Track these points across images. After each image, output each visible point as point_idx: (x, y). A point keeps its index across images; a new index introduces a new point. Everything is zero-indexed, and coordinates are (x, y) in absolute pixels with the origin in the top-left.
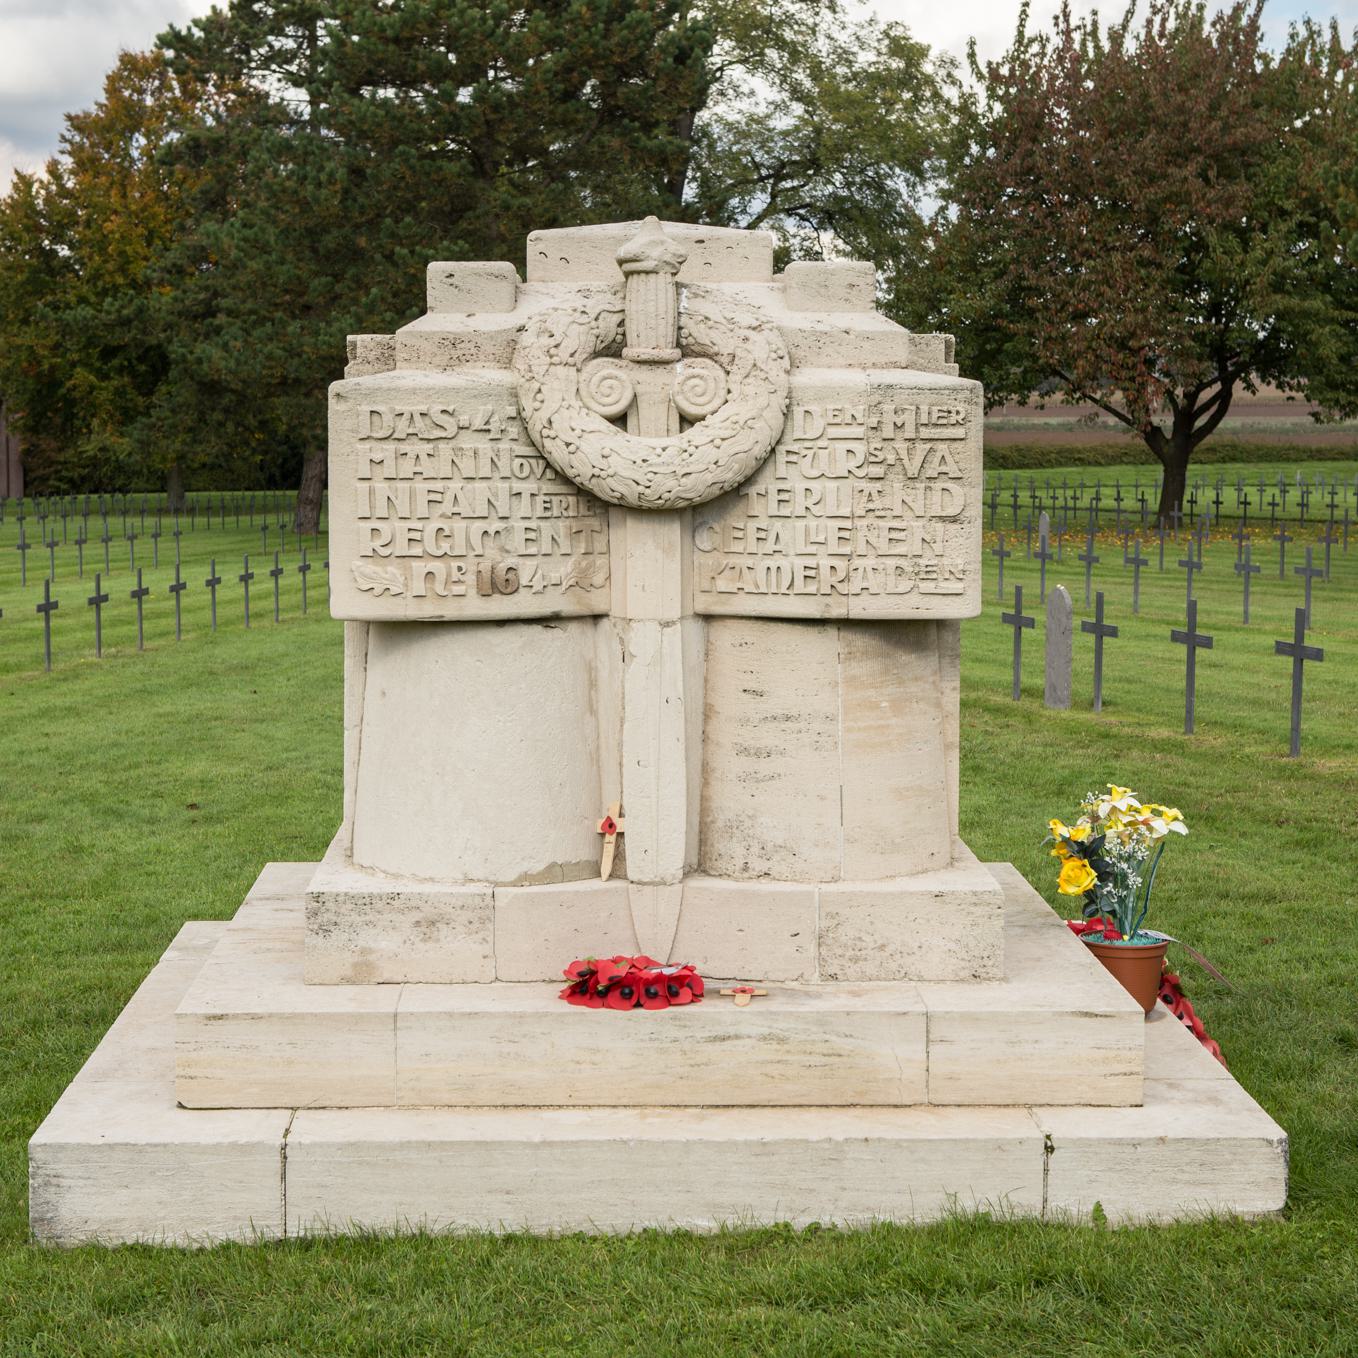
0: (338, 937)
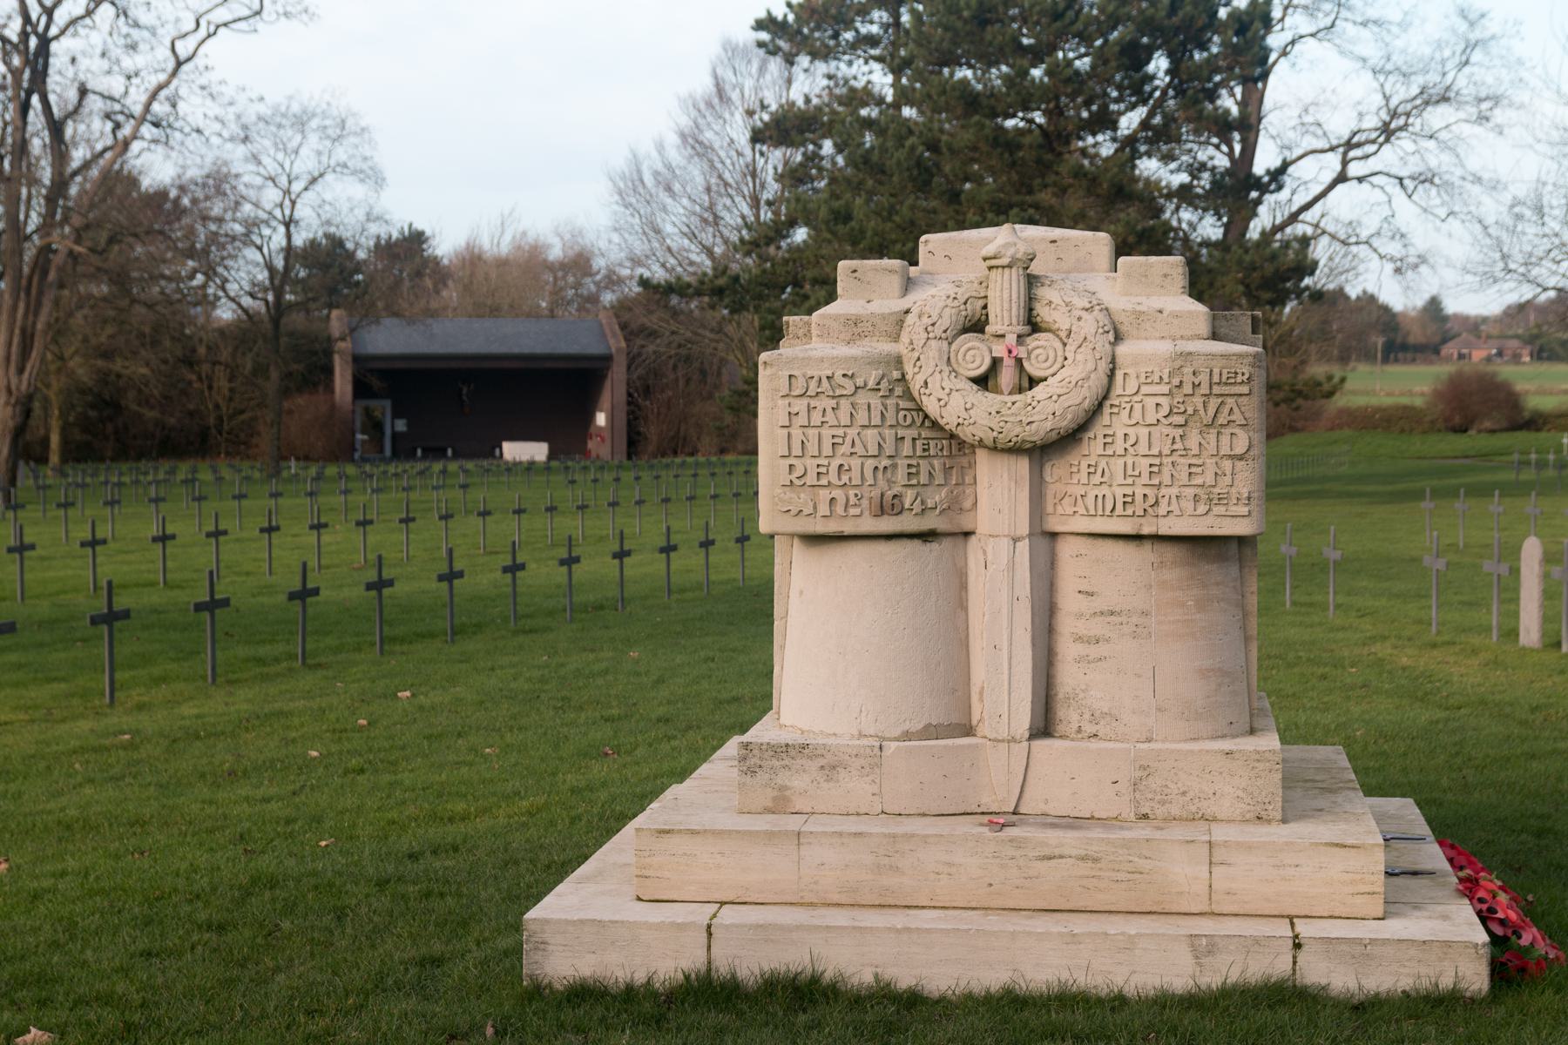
0: (762, 777)
